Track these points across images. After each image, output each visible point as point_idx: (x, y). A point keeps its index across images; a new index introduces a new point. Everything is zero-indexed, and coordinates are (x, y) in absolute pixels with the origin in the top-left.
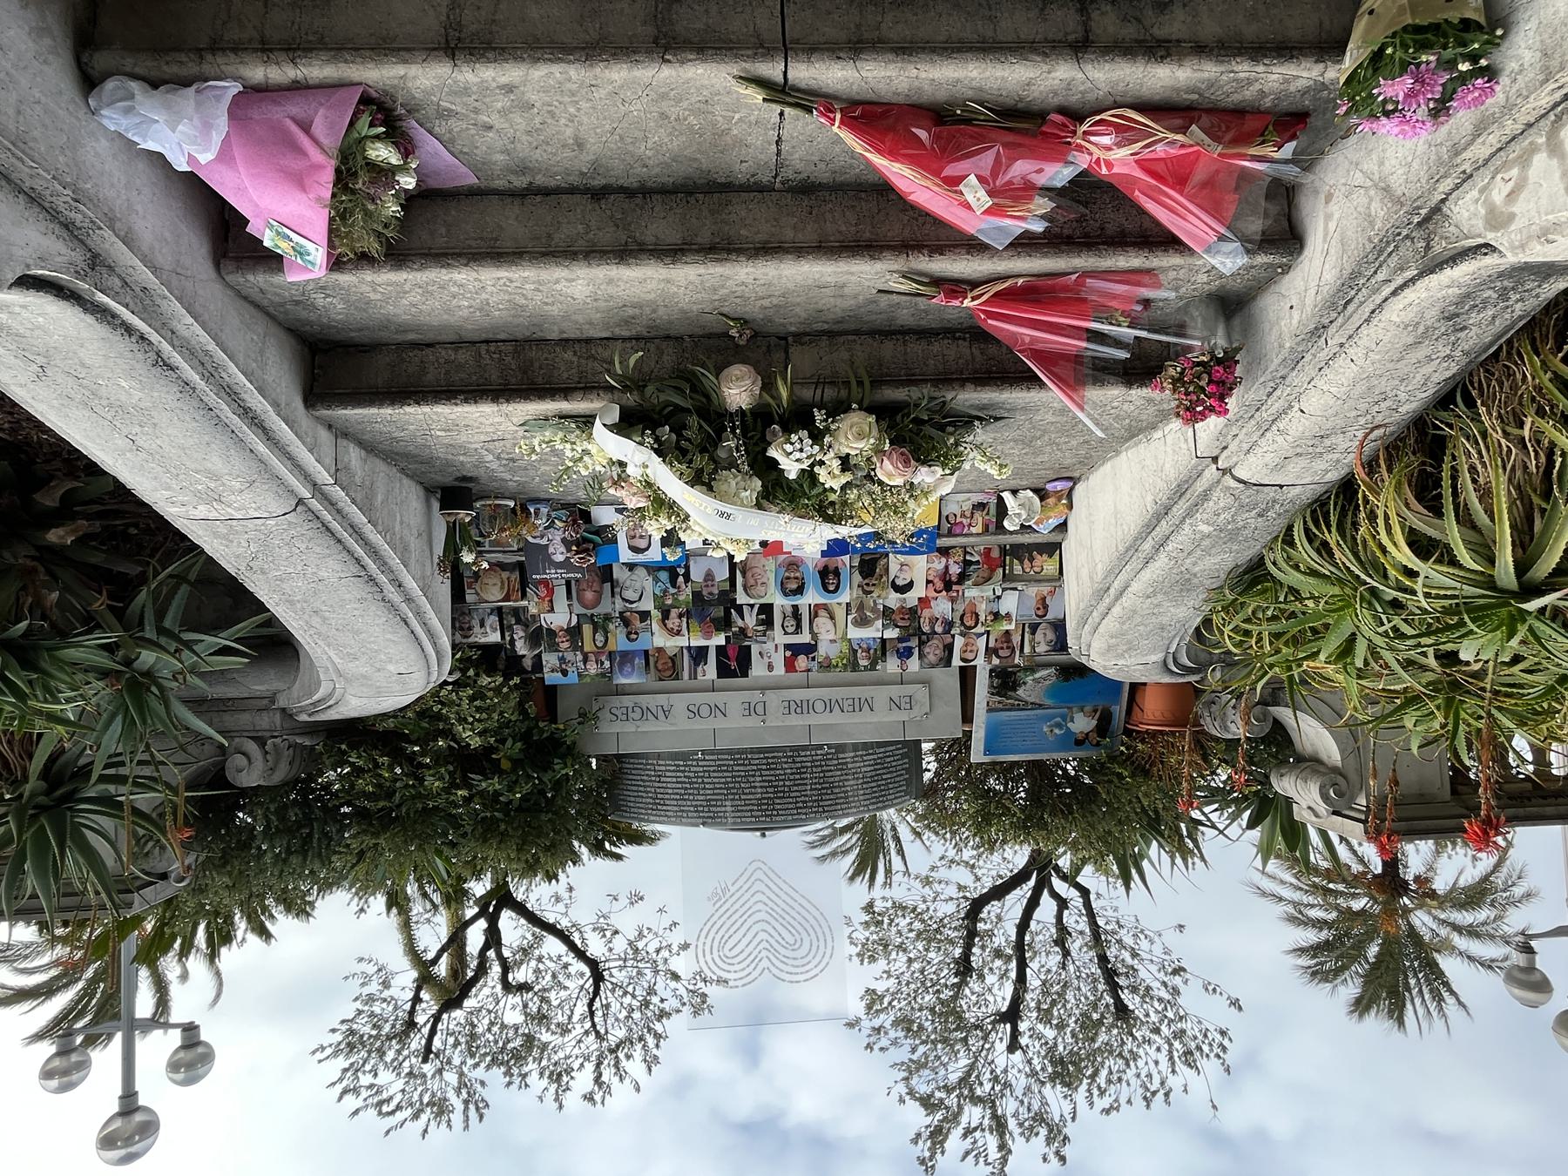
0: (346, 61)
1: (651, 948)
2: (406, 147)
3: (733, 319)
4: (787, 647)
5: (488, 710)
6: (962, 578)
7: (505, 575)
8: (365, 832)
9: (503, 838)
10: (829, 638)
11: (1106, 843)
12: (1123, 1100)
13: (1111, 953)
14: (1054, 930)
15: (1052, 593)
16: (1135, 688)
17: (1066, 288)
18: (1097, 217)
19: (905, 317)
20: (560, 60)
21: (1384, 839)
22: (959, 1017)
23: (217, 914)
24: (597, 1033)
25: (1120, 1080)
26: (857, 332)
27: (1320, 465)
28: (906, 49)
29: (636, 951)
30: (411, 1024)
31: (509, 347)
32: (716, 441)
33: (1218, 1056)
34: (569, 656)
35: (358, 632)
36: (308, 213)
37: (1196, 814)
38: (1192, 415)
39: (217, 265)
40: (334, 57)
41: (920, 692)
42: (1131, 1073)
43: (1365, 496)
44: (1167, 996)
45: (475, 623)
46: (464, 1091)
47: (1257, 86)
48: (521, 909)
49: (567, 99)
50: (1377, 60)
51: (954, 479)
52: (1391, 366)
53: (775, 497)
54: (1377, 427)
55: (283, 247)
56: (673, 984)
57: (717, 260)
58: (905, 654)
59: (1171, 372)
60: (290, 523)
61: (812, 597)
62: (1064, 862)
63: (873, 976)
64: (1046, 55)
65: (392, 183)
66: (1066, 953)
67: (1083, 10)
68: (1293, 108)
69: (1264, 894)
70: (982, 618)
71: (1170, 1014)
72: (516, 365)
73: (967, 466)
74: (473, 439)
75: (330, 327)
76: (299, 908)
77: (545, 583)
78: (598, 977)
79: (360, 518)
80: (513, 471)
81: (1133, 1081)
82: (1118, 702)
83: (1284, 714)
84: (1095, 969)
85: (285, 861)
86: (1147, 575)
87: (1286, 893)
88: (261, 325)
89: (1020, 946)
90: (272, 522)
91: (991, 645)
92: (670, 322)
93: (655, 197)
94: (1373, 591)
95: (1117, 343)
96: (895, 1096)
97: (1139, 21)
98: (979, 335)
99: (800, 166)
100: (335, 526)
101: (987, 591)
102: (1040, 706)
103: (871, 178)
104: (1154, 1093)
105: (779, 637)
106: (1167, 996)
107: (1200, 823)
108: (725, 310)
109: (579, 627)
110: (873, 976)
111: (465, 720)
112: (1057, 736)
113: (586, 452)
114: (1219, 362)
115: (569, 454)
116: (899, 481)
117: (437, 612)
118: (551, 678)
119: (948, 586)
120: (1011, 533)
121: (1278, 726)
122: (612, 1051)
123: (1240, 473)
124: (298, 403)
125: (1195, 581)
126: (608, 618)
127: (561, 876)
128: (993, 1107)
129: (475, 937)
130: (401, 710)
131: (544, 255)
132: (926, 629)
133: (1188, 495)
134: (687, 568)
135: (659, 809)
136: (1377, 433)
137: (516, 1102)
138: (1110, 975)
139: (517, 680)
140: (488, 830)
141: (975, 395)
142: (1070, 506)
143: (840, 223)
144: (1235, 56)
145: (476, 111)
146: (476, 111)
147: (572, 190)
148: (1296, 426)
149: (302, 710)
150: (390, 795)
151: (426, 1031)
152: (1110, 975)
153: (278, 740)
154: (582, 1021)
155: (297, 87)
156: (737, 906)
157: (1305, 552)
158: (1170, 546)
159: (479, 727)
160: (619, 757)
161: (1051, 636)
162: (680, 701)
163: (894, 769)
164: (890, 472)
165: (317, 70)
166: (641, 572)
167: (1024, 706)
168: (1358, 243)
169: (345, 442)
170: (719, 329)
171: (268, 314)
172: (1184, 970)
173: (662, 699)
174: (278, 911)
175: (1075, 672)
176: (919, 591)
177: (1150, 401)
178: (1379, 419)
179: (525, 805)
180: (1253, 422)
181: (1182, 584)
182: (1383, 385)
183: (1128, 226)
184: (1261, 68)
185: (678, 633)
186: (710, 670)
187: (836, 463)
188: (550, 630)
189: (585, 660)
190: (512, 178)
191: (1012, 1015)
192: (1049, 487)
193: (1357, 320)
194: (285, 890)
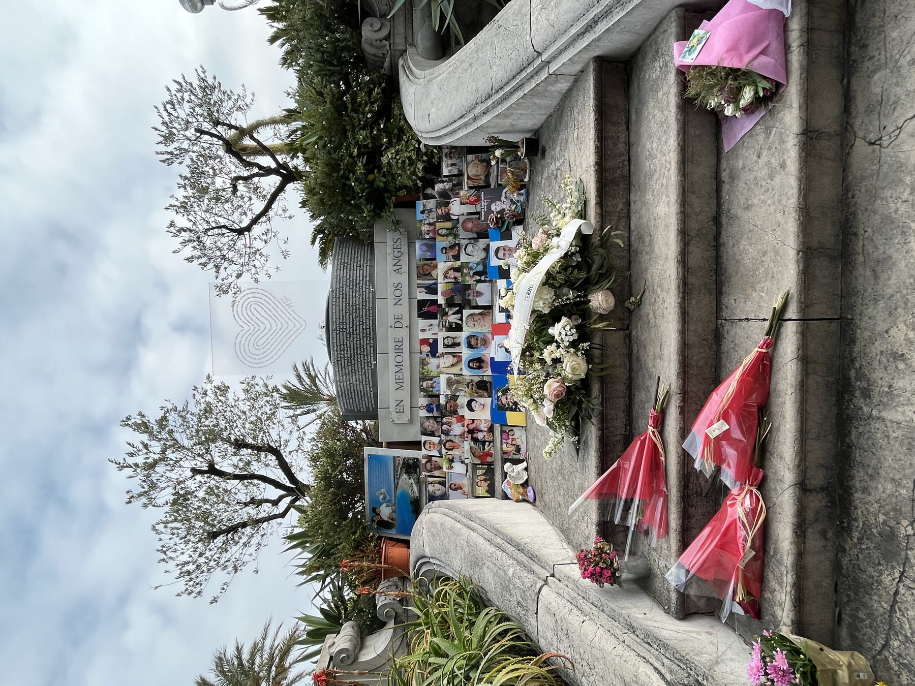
0: (801, 74)
1: (256, 262)
2: (749, 110)
3: (641, 298)
4: (436, 341)
5: (403, 168)
6: (475, 440)
7: (483, 177)
8: (334, 95)
9: (328, 175)
10: (441, 365)
11: (316, 524)
12: (161, 536)
13: (248, 530)
14: (259, 498)
15: (464, 493)
16: (407, 544)
17: (658, 485)
18: (701, 499)
19: (640, 396)
20: (800, 194)
21: (324, 678)
22: (214, 441)
23: (287, 12)
24: (209, 230)
25: (173, 534)
26: (631, 370)
27: (550, 635)
28: (803, 387)
29: (255, 253)
30: (217, 123)
31: (626, 172)
32: (571, 286)
33: (187, 590)
34: (433, 215)
35: (457, 89)
36: (714, 54)
37: (328, 580)
38: (583, 559)
39: (680, 6)
40: (803, 68)
41: (406, 418)
42: (177, 540)
43: (531, 660)
44: (222, 561)
45: (454, 161)
46: (178, 152)
47: (777, 587)
48: (281, 189)
49: (776, 198)
50: (794, 651)
51: (544, 425)
52: (611, 670)
53: (538, 322)
54: (573, 666)
55: (693, 41)
56: (235, 275)
57: (679, 286)
58: (429, 409)
59: (607, 548)
60: (527, 48)
61: (466, 353)
62: (303, 502)
63: (237, 391)
64: (799, 466)
65: (728, 102)
66: (246, 505)
67: (823, 489)
68: (763, 610)
69: (266, 630)
70: (450, 452)
71: (212, 563)
72: (616, 176)
73: (552, 433)
74: (571, 153)
75: (641, 72)
76: (288, 60)
77: (478, 199)
78: (240, 232)
79: (527, 89)
80: (549, 178)
81: (172, 542)
82: (398, 533)
83: (391, 624)
84: (238, 520)
85: (318, 50)
86: (481, 541)
87: (268, 643)
88: (644, 31)
89: (253, 476)
90: (528, 38)
91: (434, 459)
92: (640, 263)
93: (714, 252)
94: (476, 666)
95: (624, 517)
96: (165, 404)
97: (816, 520)
98: (628, 440)
99: (732, 333)
100: (524, 74)
101: (467, 454)
102: (396, 487)
103: (723, 375)
104: (165, 553)
105: (442, 335)
106: (222, 561)
107: (324, 582)
108: (647, 293)
109: (450, 220)
110: (237, 391)
111: (397, 154)
112: (380, 495)
113: (564, 215)
114: (613, 574)
115: (564, 206)
116: (546, 391)
117: (466, 136)
118: (420, 204)
119: (471, 432)
120: (503, 467)
121: (382, 625)
122: (198, 238)
123: (545, 590)
124: (598, 52)
125: (477, 569)
126: (456, 236)
127: (304, 210)
128: (161, 460)
129: (266, 161)
130: (405, 117)
131: (684, 188)
132: (445, 420)
133: (531, 561)
134: (485, 281)
135: (341, 266)
136: (569, 665)
137: (171, 183)
138: (234, 529)
139: (420, 184)
140: (333, 166)
141: (594, 436)
142: (517, 501)
143: (698, 356)
144: (796, 574)
145: (769, 148)
146: (769, 148)
147: (719, 205)
148: (575, 619)
149: (406, 61)
150: (355, 111)
151: (213, 131)
152: (234, 529)
153: (388, 48)
154: (215, 222)
155: (786, 48)
156: (280, 312)
157: (496, 629)
158: (499, 553)
159: (393, 162)
160: (372, 244)
161: (438, 493)
162: (404, 279)
163: (360, 402)
164: (552, 387)
165: (796, 58)
166: (483, 255)
167: (397, 478)
168: (685, 648)
169: (572, 81)
170: (634, 291)
171: (650, 36)
172: (236, 572)
173: (405, 268)
174: (287, 47)
175: (416, 508)
176: (468, 415)
177: (588, 538)
178: (577, 666)
179: (347, 188)
180: (576, 595)
181: (476, 562)
182: (599, 667)
183: (693, 521)
184: (789, 589)
185: (446, 277)
186: (422, 296)
187: (558, 355)
188: (449, 203)
189: (430, 224)
190: (728, 171)
191: (212, 470)
192: (530, 488)
193: (640, 649)
194: (299, 51)
